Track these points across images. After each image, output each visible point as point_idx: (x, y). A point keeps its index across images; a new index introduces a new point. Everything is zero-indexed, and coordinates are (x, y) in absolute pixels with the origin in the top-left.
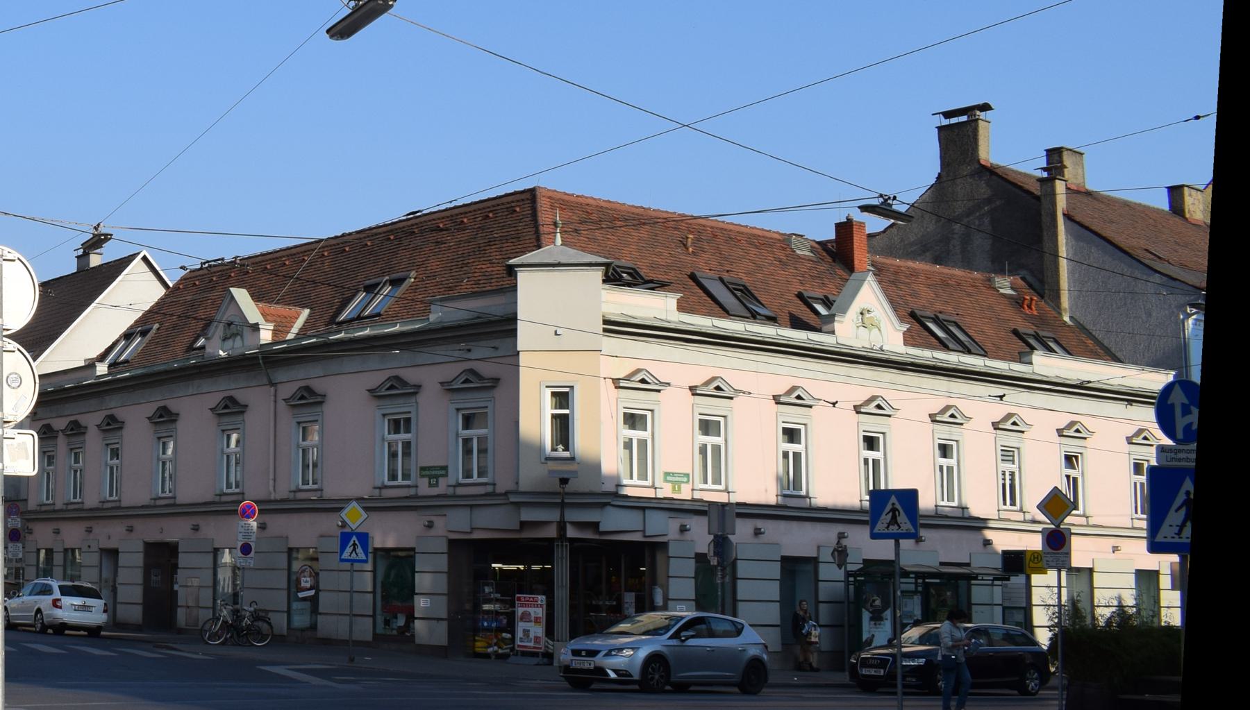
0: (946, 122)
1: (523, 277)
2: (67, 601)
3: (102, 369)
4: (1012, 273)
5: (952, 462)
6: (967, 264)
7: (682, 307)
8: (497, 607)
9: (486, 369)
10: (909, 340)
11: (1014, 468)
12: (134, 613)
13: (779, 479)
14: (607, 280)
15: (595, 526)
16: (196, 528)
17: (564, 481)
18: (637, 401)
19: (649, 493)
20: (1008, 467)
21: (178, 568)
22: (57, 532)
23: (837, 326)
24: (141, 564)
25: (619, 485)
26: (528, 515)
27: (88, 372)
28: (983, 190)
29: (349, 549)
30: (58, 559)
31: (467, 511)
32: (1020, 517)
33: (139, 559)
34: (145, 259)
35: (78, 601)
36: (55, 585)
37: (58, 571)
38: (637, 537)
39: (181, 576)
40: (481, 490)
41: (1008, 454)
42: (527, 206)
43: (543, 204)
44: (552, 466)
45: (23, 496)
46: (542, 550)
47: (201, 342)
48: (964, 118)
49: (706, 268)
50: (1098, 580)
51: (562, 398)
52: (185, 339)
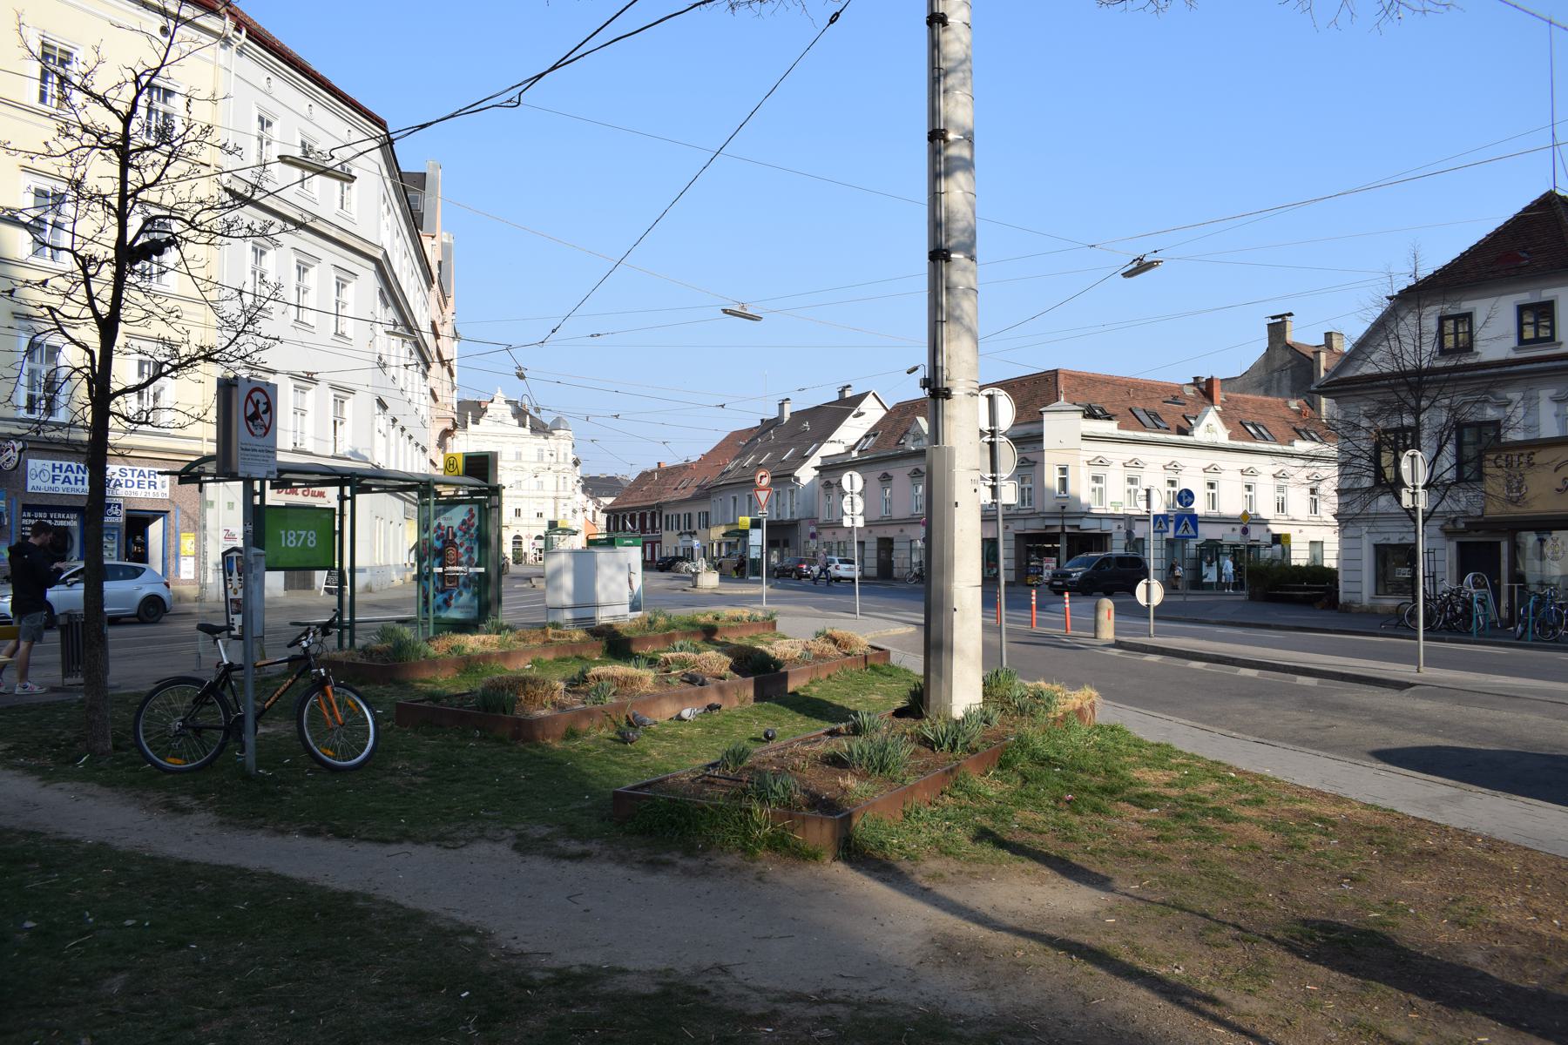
0: (1272, 321)
1: (1046, 416)
2: (842, 566)
3: (855, 454)
4: (1298, 397)
5: (1252, 493)
6: (1280, 394)
7: (1120, 427)
8: (1037, 563)
9: (1031, 457)
10: (1231, 437)
11: (1284, 495)
12: (873, 572)
13: (1166, 503)
14: (1084, 417)
15: (1078, 527)
16: (902, 531)
17: (1063, 507)
18: (1098, 471)
19: (1104, 512)
20: (1281, 495)
21: (120, 320)
22: (834, 534)
23: (1195, 432)
24: (876, 565)
25: (1090, 508)
26: (1049, 522)
27: (848, 456)
28: (1288, 356)
29: (1182, 528)
30: (835, 547)
31: (1022, 521)
32: (1286, 518)
33: (875, 546)
34: (874, 394)
35: (847, 566)
36: (836, 559)
37: (835, 552)
38: (1098, 531)
39: (894, 553)
40: (1029, 512)
41: (1280, 489)
42: (1054, 378)
43: (1061, 377)
44: (1059, 501)
45: (815, 516)
46: (1054, 538)
47: (902, 441)
48: (1280, 320)
49: (1138, 406)
50: (1325, 546)
51: (1064, 470)
52: (895, 439)
